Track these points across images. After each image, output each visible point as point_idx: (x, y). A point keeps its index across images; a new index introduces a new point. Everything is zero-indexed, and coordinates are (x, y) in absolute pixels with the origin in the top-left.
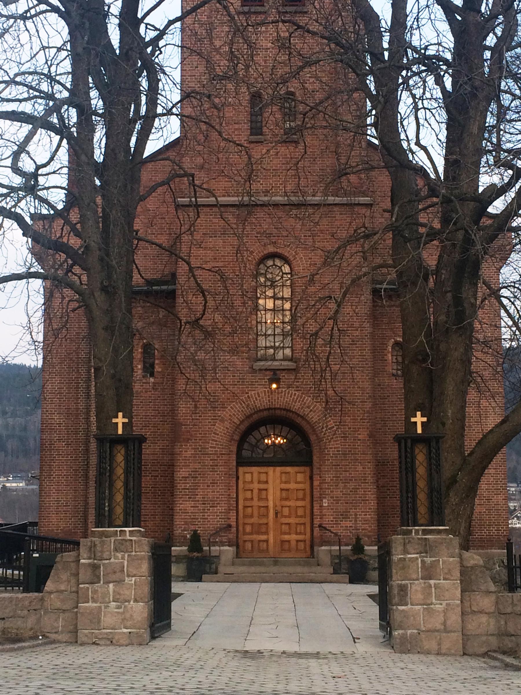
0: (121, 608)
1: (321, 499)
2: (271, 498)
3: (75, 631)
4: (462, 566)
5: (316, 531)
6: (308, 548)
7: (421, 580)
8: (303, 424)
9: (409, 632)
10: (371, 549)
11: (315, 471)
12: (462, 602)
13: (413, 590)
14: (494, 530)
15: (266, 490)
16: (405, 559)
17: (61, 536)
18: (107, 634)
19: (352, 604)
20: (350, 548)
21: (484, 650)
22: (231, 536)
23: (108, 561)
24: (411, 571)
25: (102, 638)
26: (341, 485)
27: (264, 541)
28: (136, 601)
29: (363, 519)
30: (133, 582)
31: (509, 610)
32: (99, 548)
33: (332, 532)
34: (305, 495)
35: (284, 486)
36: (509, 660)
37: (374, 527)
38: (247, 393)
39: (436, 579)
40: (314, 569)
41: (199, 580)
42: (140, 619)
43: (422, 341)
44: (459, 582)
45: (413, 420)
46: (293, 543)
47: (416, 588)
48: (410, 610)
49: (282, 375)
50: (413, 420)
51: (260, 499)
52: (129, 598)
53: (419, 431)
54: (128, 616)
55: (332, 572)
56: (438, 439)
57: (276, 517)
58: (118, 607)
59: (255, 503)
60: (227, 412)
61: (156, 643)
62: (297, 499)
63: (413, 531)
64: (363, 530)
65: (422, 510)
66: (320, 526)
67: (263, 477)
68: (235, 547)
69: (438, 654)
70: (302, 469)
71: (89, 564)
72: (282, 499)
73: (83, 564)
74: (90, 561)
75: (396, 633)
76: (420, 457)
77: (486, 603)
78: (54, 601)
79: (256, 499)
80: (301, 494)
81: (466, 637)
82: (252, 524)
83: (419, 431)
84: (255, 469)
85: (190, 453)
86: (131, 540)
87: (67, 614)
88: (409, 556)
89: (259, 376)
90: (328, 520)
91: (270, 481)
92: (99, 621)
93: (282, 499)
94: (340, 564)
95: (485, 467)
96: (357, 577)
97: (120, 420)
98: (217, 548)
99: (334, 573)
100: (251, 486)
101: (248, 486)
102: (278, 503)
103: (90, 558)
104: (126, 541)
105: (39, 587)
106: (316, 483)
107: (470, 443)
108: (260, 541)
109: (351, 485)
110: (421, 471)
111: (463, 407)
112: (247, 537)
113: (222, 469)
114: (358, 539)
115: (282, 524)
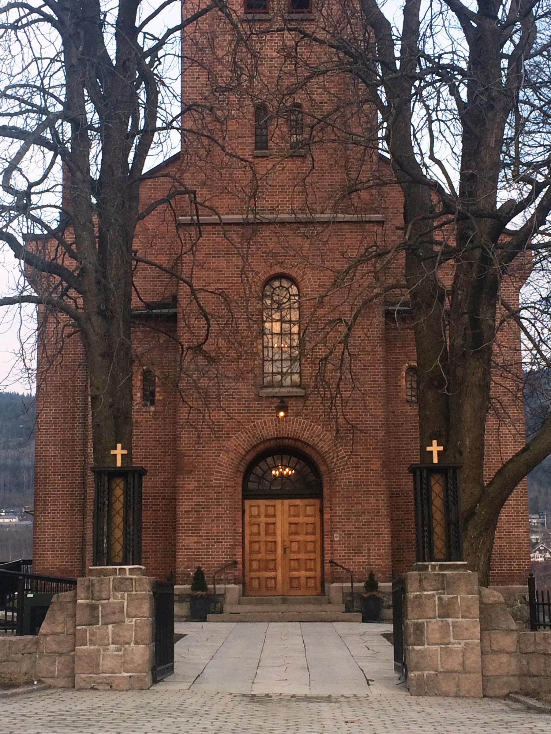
0: (121, 650)
1: (332, 532)
2: (279, 533)
3: (72, 676)
4: (481, 603)
5: (327, 566)
7: (438, 619)
8: (313, 454)
9: (426, 673)
10: (385, 586)
11: (327, 504)
12: (481, 640)
13: (430, 630)
15: (274, 524)
16: (420, 597)
17: (58, 575)
18: (105, 678)
20: (362, 584)
21: (505, 691)
22: (237, 573)
23: (107, 601)
24: (427, 609)
25: (101, 683)
26: (353, 518)
27: (271, 578)
28: (136, 643)
29: (376, 554)
30: (133, 623)
31: (532, 649)
32: (97, 588)
33: (344, 568)
34: (314, 529)
35: (293, 520)
36: (532, 702)
37: (388, 562)
38: (252, 422)
39: (454, 617)
41: (203, 619)
42: (141, 662)
43: (437, 366)
44: (478, 620)
45: (429, 449)
46: (303, 581)
47: (433, 627)
48: (428, 651)
49: (291, 403)
50: (429, 449)
52: (127, 641)
53: (435, 461)
54: (128, 658)
55: (344, 610)
56: (456, 469)
57: (285, 552)
58: (119, 650)
59: (263, 537)
60: (232, 442)
61: (158, 687)
62: (307, 534)
63: (430, 567)
64: (376, 565)
65: (439, 544)
66: (331, 562)
67: (271, 511)
68: (241, 586)
69: (456, 697)
70: (312, 501)
71: (87, 605)
72: (291, 534)
73: (81, 604)
74: (88, 601)
75: (412, 675)
76: (437, 488)
77: (507, 642)
78: (49, 644)
79: (263, 532)
80: (310, 529)
81: (486, 679)
83: (435, 461)
84: (262, 503)
85: (193, 484)
86: (131, 579)
87: (62, 659)
88: (426, 593)
90: (340, 555)
91: (278, 514)
92: (98, 665)
93: (291, 534)
94: (352, 602)
95: (506, 498)
96: (372, 616)
97: (119, 451)
98: (223, 586)
99: (346, 612)
100: (257, 520)
101: (254, 520)
102: (287, 540)
103: (87, 598)
104: (128, 579)
105: (33, 629)
106: (326, 516)
108: (267, 578)
109: (365, 518)
110: (438, 502)
112: (253, 574)
113: (227, 502)
114: (372, 575)
115: (291, 560)
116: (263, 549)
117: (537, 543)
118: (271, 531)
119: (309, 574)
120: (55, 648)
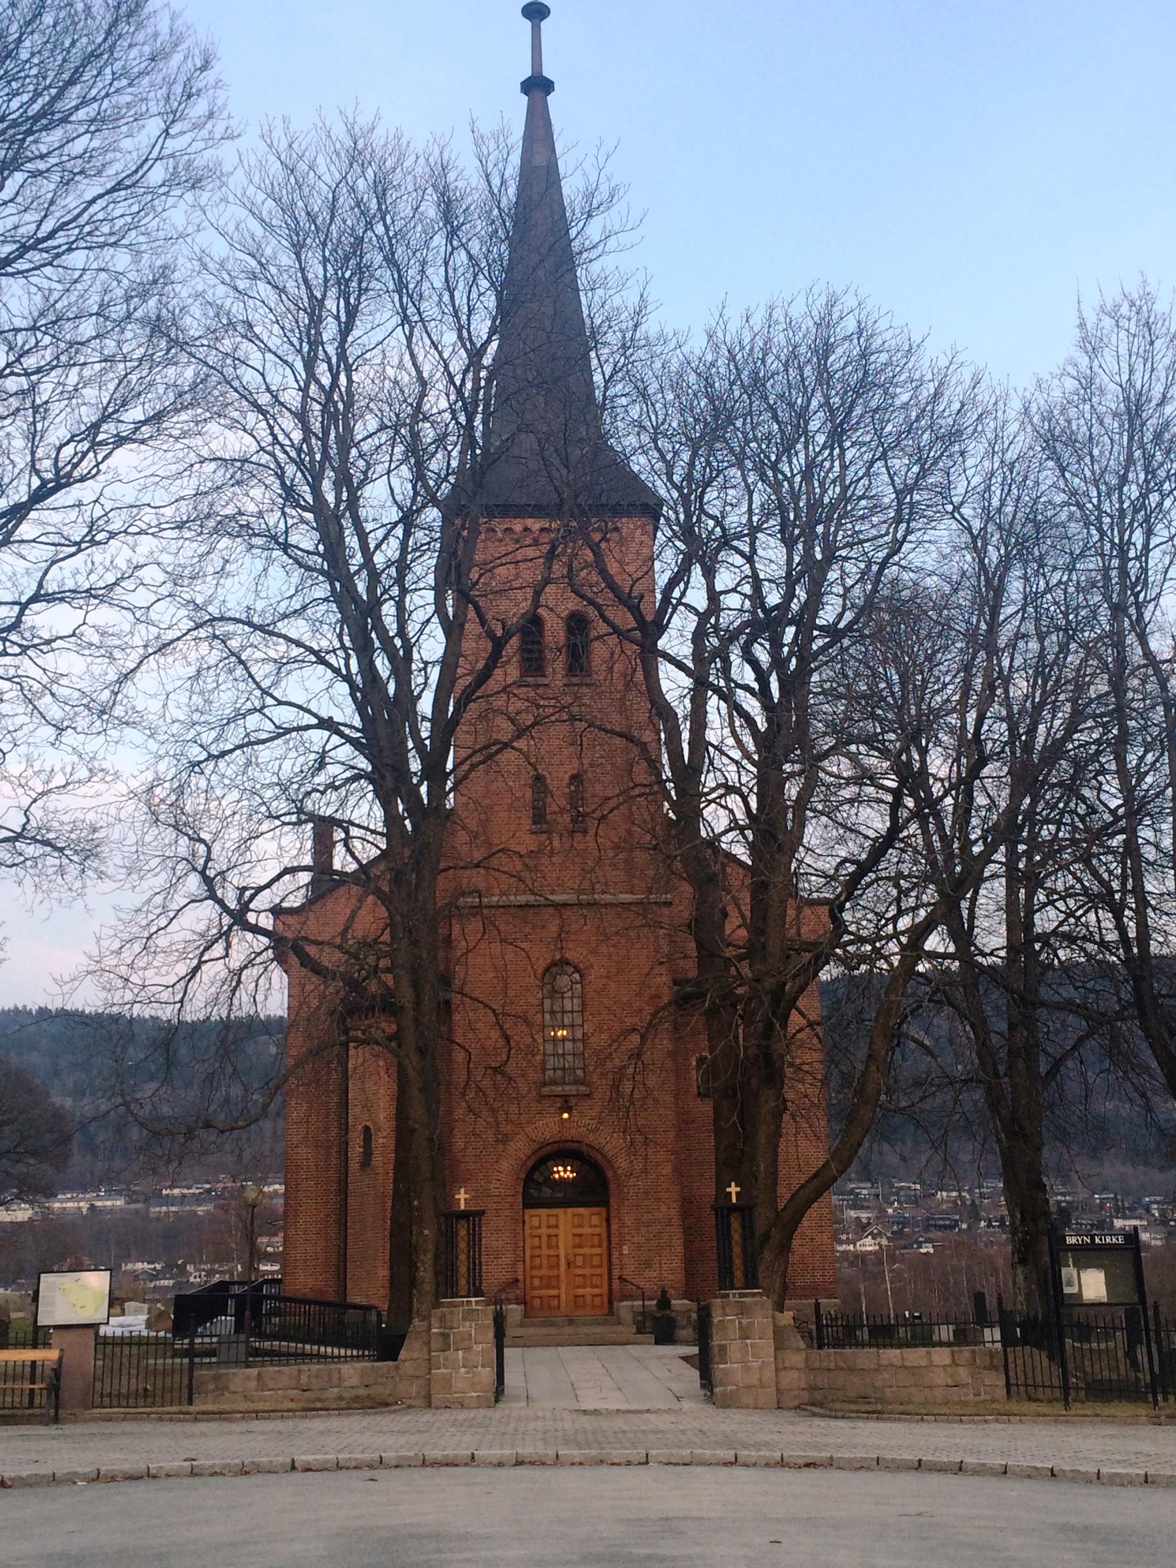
1: (620, 1245)
2: (562, 1246)
5: (616, 1282)
6: (606, 1305)
10: (679, 1304)
11: (613, 1213)
14: (819, 1274)
17: (310, 1296)
19: (661, 1370)
21: (797, 1403)
29: (668, 1268)
31: (817, 1365)
37: (681, 1276)
39: (752, 1333)
40: (614, 1328)
46: (588, 1299)
47: (734, 1348)
49: (573, 1101)
51: (549, 1247)
56: (751, 1208)
59: (545, 1251)
65: (738, 1274)
67: (553, 1221)
70: (596, 1210)
71: (441, 1334)
75: (717, 1390)
76: (735, 1225)
78: (408, 1368)
79: (544, 1246)
80: (596, 1239)
82: (541, 1278)
84: (544, 1212)
87: (420, 1382)
89: (547, 1102)
95: (800, 1221)
96: (664, 1334)
106: (614, 1227)
107: (784, 1194)
110: (736, 1237)
111: (775, 1161)
113: (507, 1213)
114: (664, 1292)
116: (545, 1262)
117: (869, 1224)
118: (554, 1243)
119: (597, 1291)
120: (411, 1372)
